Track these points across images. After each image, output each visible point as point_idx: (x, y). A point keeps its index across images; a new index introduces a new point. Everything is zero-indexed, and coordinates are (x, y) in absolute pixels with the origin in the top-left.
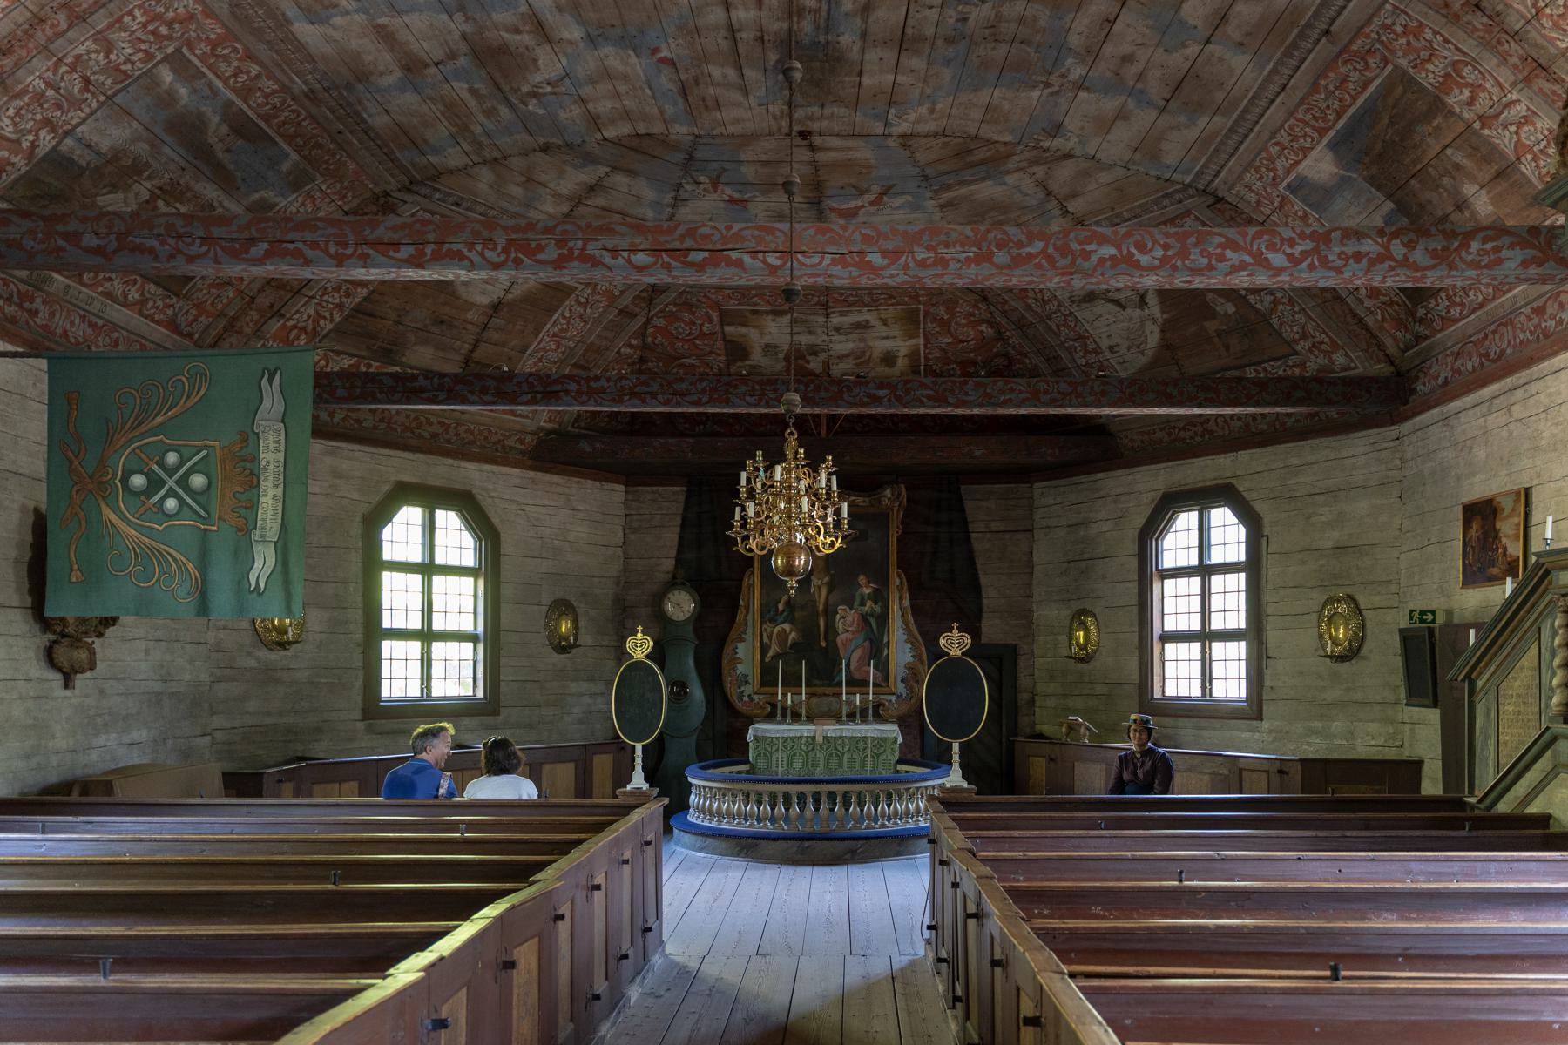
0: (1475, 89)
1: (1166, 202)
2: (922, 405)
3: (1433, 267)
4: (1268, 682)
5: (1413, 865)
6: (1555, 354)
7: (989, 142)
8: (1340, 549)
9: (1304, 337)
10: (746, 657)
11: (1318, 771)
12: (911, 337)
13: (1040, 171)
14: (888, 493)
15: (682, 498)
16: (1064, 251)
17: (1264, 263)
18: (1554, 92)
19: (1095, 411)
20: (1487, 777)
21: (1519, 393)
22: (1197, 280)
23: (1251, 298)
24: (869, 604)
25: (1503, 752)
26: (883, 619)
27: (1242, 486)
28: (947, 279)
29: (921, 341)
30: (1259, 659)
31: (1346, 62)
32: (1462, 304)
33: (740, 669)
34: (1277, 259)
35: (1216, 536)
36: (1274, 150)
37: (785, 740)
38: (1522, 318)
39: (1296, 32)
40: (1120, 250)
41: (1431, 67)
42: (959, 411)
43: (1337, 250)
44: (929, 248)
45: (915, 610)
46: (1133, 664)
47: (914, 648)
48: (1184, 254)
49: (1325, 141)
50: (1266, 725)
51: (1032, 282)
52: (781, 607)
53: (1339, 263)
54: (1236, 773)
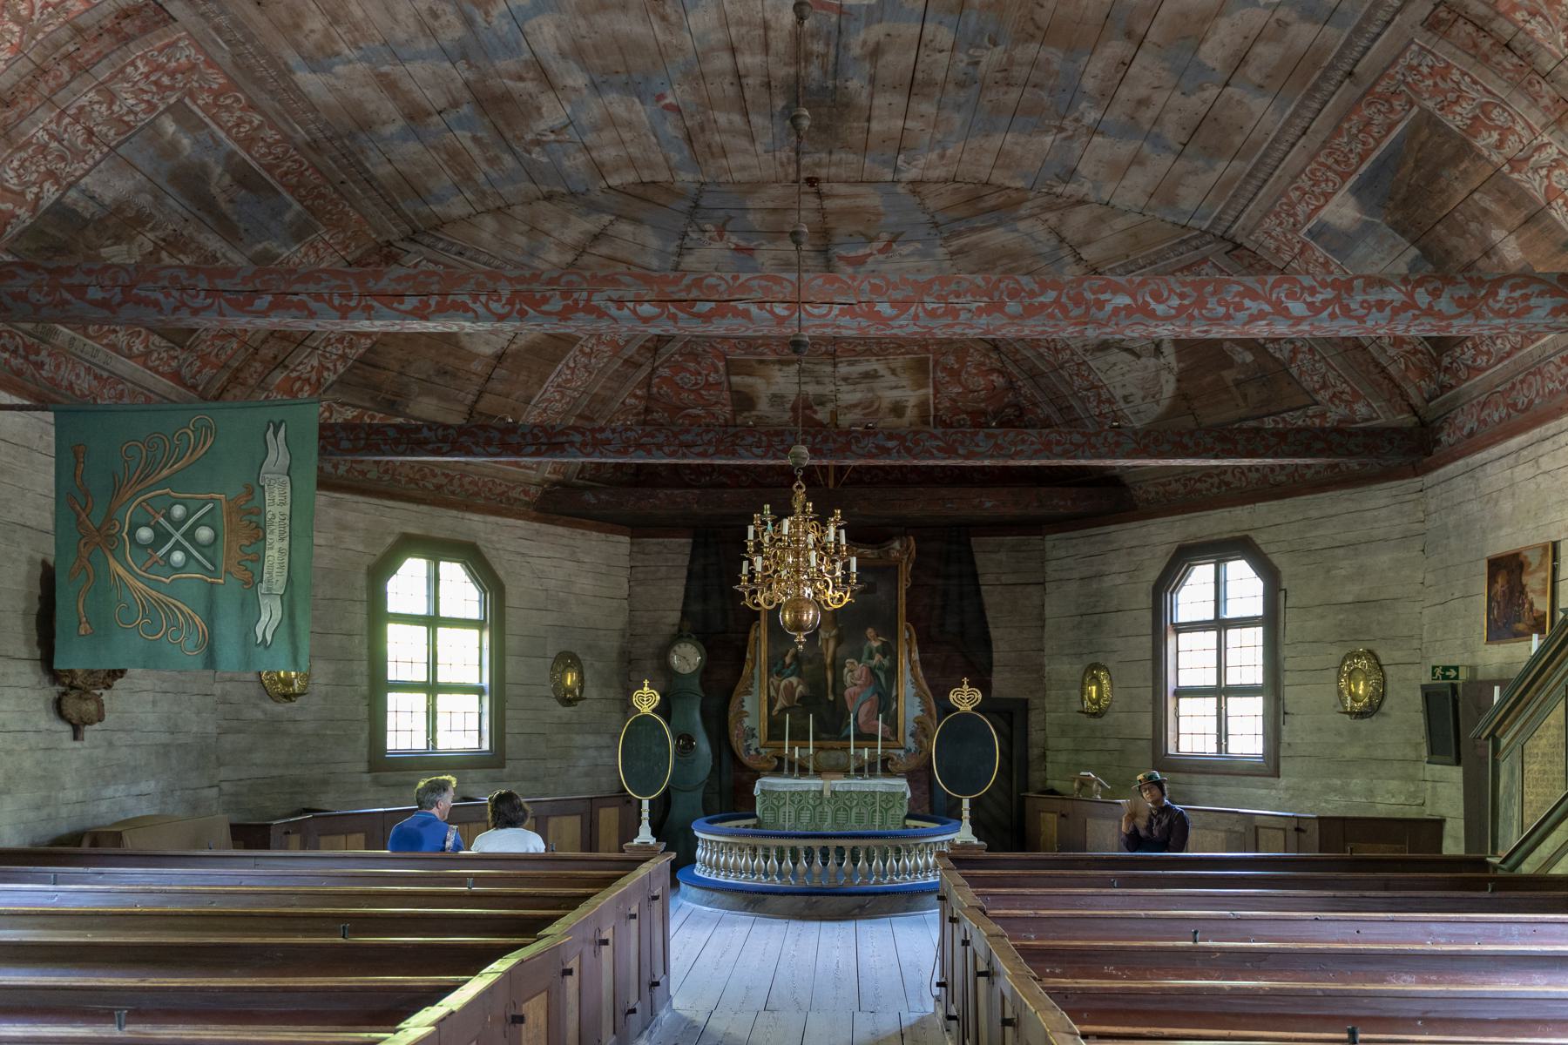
0: (1505, 132)
1: (1183, 248)
2: (933, 457)
4: (1285, 738)
5: (1434, 927)
7: (1001, 188)
8: (1360, 603)
9: (1324, 386)
10: (752, 710)
11: (1336, 830)
12: (921, 386)
13: (1052, 218)
14: (897, 545)
15: (688, 550)
17: (1283, 312)
19: (1108, 462)
20: (1511, 837)
21: (1548, 445)
22: (1215, 329)
24: (878, 657)
25: (1527, 812)
26: (892, 672)
27: (1260, 539)
28: (958, 330)
29: (931, 391)
32: (1489, 353)
33: (747, 722)
34: (1297, 308)
35: (1232, 589)
36: (1295, 195)
37: (793, 794)
38: (1552, 368)
39: (1318, 74)
40: (1135, 300)
41: (1458, 109)
42: (970, 463)
43: (1359, 298)
44: (940, 298)
45: (925, 664)
46: (1147, 719)
47: (924, 702)
48: (1201, 303)
49: (1348, 185)
50: (1283, 782)
51: (1043, 332)
52: (788, 660)
54: (1252, 832)
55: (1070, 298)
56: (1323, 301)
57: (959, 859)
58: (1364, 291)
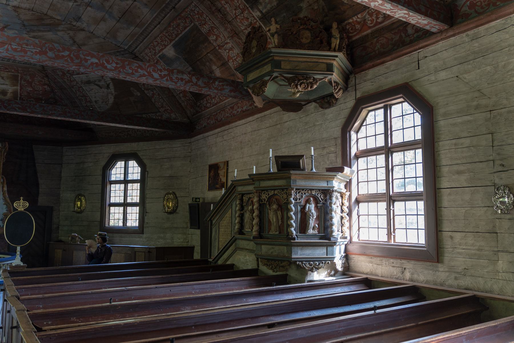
0: (218, 37)
1: (118, 54)
2: (16, 110)
3: (204, 87)
4: (146, 221)
5: (195, 286)
6: (236, 121)
7: (51, 18)
8: (171, 177)
9: (162, 107)
11: (162, 252)
12: (14, 85)
13: (71, 33)
16: (77, 57)
17: (152, 76)
18: (239, 42)
19: (88, 122)
20: (215, 253)
21: (226, 132)
22: (128, 77)
23: (146, 91)
25: (220, 244)
27: (140, 154)
28: (26, 58)
29: (19, 88)
30: (143, 213)
31: (179, 19)
32: (210, 103)
34: (156, 75)
35: (130, 170)
36: (156, 43)
38: (227, 109)
39: (164, 5)
40: (100, 61)
41: (205, 27)
42: (32, 115)
43: (175, 76)
44: (19, 44)
46: (98, 214)
48: (123, 67)
49: (172, 44)
50: (144, 236)
51: (63, 66)
53: (176, 80)
54: (133, 254)
55: (74, 56)
56: (164, 75)
57: (13, 273)
58: (177, 74)
